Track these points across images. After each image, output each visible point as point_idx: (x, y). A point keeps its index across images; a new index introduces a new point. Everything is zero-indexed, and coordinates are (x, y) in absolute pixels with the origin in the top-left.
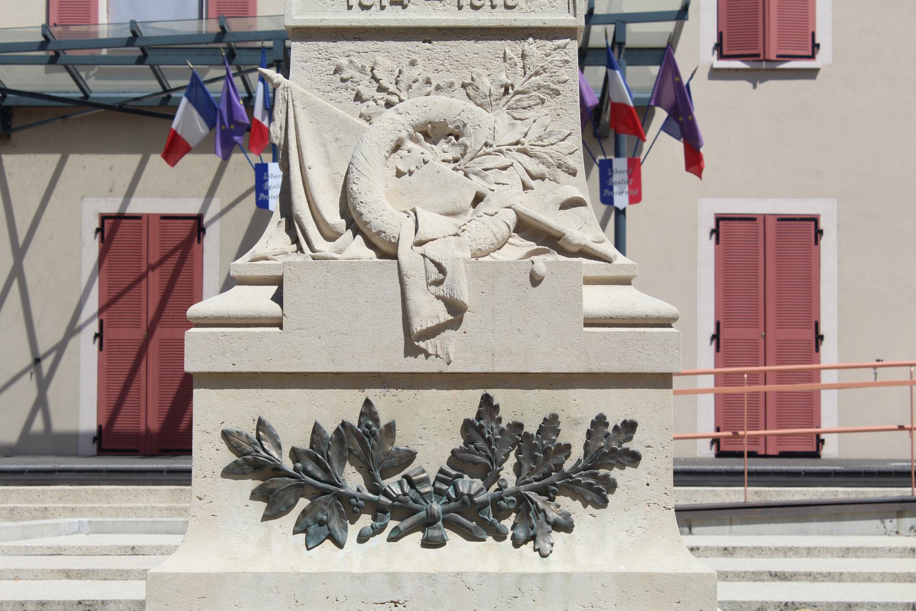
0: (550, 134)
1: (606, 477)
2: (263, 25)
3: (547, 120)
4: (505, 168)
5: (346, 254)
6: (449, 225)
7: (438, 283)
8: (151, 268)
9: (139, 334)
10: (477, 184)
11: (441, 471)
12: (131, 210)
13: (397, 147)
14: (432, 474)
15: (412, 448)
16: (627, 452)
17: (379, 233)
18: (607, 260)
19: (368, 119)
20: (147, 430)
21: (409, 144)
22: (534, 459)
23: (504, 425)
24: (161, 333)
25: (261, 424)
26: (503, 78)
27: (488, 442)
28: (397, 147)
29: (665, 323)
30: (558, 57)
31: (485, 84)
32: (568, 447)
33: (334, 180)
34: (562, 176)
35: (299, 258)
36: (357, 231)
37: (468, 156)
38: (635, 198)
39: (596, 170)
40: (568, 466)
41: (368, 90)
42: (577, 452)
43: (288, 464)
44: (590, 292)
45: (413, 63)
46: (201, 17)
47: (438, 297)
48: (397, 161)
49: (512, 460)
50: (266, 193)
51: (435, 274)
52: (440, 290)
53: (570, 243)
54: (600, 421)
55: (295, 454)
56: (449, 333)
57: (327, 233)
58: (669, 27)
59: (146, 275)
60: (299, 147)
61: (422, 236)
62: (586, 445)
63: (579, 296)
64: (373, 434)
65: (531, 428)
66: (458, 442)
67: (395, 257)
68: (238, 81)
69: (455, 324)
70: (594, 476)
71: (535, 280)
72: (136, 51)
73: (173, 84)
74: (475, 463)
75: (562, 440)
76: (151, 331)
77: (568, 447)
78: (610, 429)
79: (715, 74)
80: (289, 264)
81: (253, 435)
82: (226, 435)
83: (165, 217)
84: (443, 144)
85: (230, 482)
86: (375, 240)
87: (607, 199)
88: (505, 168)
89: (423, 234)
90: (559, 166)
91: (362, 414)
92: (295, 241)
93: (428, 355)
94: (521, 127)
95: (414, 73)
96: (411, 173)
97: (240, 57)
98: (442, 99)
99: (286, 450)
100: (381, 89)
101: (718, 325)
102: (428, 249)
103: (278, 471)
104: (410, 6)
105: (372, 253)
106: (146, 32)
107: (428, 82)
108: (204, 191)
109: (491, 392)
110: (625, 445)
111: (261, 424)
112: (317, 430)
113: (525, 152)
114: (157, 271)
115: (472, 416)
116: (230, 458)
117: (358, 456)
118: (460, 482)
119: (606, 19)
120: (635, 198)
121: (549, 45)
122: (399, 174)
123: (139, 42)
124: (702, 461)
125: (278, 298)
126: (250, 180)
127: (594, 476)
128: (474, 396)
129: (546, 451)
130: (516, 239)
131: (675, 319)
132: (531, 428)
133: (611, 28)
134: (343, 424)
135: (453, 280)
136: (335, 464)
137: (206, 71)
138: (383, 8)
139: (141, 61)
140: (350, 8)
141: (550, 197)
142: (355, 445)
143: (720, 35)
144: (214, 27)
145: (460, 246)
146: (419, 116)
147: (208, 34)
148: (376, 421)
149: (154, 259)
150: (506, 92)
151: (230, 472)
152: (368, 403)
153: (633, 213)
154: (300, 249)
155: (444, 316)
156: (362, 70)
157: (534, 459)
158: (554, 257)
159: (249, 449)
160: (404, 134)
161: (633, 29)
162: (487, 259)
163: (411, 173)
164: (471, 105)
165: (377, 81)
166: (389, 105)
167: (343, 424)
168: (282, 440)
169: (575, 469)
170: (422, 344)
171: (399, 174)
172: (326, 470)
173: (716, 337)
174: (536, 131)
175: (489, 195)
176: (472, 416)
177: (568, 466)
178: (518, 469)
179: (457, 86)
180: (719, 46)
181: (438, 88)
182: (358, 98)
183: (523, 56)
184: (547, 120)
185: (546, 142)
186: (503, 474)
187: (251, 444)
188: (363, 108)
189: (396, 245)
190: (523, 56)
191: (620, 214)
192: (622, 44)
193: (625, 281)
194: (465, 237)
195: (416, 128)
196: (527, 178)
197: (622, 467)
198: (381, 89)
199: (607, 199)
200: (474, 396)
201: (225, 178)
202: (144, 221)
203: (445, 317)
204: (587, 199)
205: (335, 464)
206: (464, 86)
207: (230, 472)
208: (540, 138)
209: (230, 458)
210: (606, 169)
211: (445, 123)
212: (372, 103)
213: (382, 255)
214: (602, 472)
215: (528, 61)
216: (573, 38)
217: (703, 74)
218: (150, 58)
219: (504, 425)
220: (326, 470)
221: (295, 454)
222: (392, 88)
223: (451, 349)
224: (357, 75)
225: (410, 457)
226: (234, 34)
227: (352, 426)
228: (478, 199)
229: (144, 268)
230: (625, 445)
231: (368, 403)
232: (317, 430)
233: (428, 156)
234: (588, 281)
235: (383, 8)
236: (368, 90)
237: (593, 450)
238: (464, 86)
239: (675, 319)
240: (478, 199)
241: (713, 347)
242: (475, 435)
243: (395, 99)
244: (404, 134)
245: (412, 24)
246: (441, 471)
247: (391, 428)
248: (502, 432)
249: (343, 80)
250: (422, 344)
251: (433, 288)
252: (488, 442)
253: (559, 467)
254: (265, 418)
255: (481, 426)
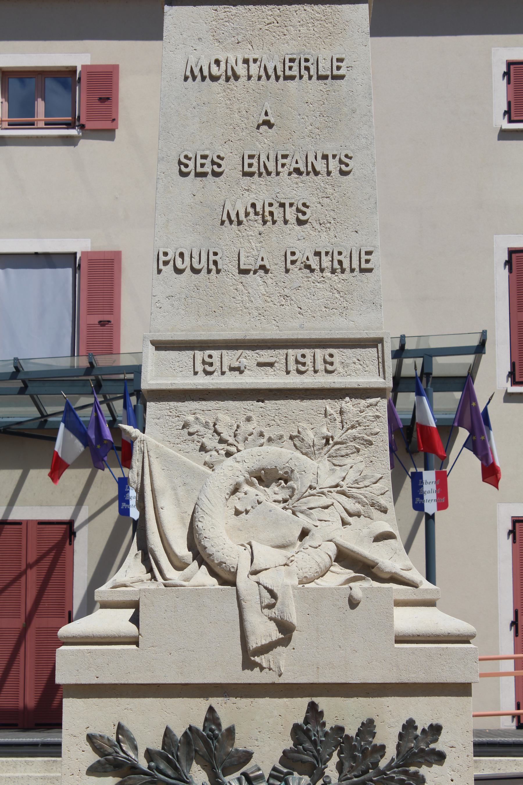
0: (365, 478)
1: (416, 774)
2: (125, 361)
3: (362, 466)
4: (326, 507)
5: (192, 582)
6: (280, 556)
7: (270, 606)
8: (30, 566)
9: (19, 623)
10: (304, 521)
11: (274, 769)
12: (14, 516)
13: (236, 490)
14: (266, 771)
15: (249, 749)
16: (433, 751)
17: (221, 563)
18: (414, 585)
19: (211, 466)
20: (25, 707)
21: (246, 488)
22: (354, 758)
23: (327, 728)
24: (36, 622)
25: (120, 729)
26: (325, 431)
27: (314, 743)
28: (236, 490)
29: (464, 639)
30: (370, 413)
31: (310, 436)
32: (382, 748)
33: (182, 519)
34: (375, 513)
35: (152, 586)
36: (201, 562)
37: (295, 497)
38: (443, 505)
39: (408, 483)
40: (383, 764)
41: (211, 442)
42: (391, 752)
43: (143, 764)
44: (399, 612)
45: (249, 419)
46: (73, 355)
47: (271, 619)
48: (236, 502)
49: (335, 759)
50: (128, 502)
51: (268, 599)
52: (273, 613)
53: (382, 571)
54: (410, 725)
55: (149, 754)
56: (280, 649)
57: (177, 563)
58: (470, 359)
59: (25, 572)
60: (150, 466)
61: (257, 566)
62: (398, 746)
63: (390, 617)
64: (216, 737)
65: (351, 731)
66: (289, 744)
67: (233, 584)
68: (104, 407)
69: (285, 642)
70: (406, 773)
71: (353, 603)
72: (18, 384)
73: (50, 410)
74: (303, 762)
75: (377, 741)
76: (29, 620)
77: (382, 748)
78: (419, 732)
79: (509, 397)
80: (145, 590)
81: (114, 738)
82: (90, 738)
83: (41, 523)
84: (274, 487)
85: (94, 779)
86: (217, 569)
87: (418, 506)
88: (326, 507)
89: (259, 564)
90: (373, 505)
91: (206, 719)
92: (150, 570)
93: (262, 669)
94: (340, 473)
95: (249, 427)
96: (247, 512)
97: (106, 387)
98: (273, 449)
99: (142, 751)
100: (222, 441)
101: (516, 613)
102: (262, 577)
103: (134, 769)
104: (246, 372)
105: (214, 581)
106: (27, 368)
107: (261, 435)
108: (75, 501)
109: (316, 700)
110: (432, 746)
111: (120, 729)
112: (168, 733)
113: (343, 493)
114: (35, 569)
115: (300, 721)
116: (93, 758)
117: (202, 756)
118: (290, 778)
119: (415, 354)
120: (443, 505)
121: (363, 403)
122: (237, 513)
123: (21, 376)
124: (505, 733)
125: (135, 620)
126: (114, 491)
127: (406, 773)
128: (303, 703)
129: (364, 751)
130: (337, 568)
131: (473, 636)
132: (351, 731)
133: (419, 361)
134: (190, 728)
135: (283, 604)
136: (184, 763)
137: (77, 400)
138: (223, 373)
139: (22, 391)
140: (196, 373)
141: (365, 531)
142: (200, 746)
143: (513, 365)
144: (83, 362)
145: (289, 574)
146: (254, 464)
147: (79, 369)
148: (219, 725)
149: (32, 559)
150: (327, 443)
151: (93, 771)
152: (211, 710)
153: (440, 517)
154: (154, 577)
155: (276, 635)
156: (206, 425)
157: (354, 758)
158: (370, 584)
159: (110, 750)
160: (241, 479)
161: (439, 361)
162: (312, 585)
163: (247, 512)
164: (298, 454)
165: (219, 434)
166: (228, 454)
167: (190, 728)
168: (139, 742)
169: (389, 767)
170: (257, 659)
171: (237, 513)
172: (176, 769)
173: (515, 624)
174: (352, 476)
175: (314, 530)
176: (300, 721)
177: (383, 764)
178: (340, 767)
179: (286, 438)
180: (512, 374)
181: (270, 440)
182: (203, 448)
183: (341, 413)
184: (362, 466)
185: (361, 485)
186: (327, 772)
187: (112, 746)
188: (207, 457)
189: (235, 574)
190: (341, 413)
191: (430, 518)
192: (429, 374)
193: (431, 604)
194: (293, 566)
195: (251, 474)
196: (345, 515)
197: (430, 765)
198: (222, 441)
199: (418, 506)
200: (303, 703)
201: (93, 489)
202: (24, 526)
203: (276, 635)
204: (397, 533)
205: (184, 763)
206: (292, 438)
207: (93, 771)
208: (356, 482)
209: (93, 758)
210: (417, 479)
211: (276, 470)
212: (214, 453)
213: (223, 582)
214: (412, 769)
215: (345, 417)
216: (383, 397)
217: (499, 397)
218: (30, 389)
219: (327, 728)
220: (176, 769)
221: (149, 754)
222: (231, 440)
223: (282, 663)
224: (202, 429)
225: (247, 756)
226: (101, 368)
227: (197, 730)
228: (304, 533)
229: (24, 567)
230: (432, 746)
231: (211, 710)
232: (168, 733)
233: (262, 498)
234: (399, 604)
235: (223, 373)
236: (211, 442)
237: (404, 750)
238: (292, 438)
239: (473, 636)
240: (304, 533)
241: (512, 633)
242: (305, 738)
243: (233, 449)
244: (241, 479)
245: (248, 387)
246: (274, 769)
247: (231, 731)
248: (326, 734)
249: (190, 434)
250: (257, 659)
251: (266, 611)
252: (314, 743)
253: (375, 765)
254: (124, 723)
255: (308, 730)
